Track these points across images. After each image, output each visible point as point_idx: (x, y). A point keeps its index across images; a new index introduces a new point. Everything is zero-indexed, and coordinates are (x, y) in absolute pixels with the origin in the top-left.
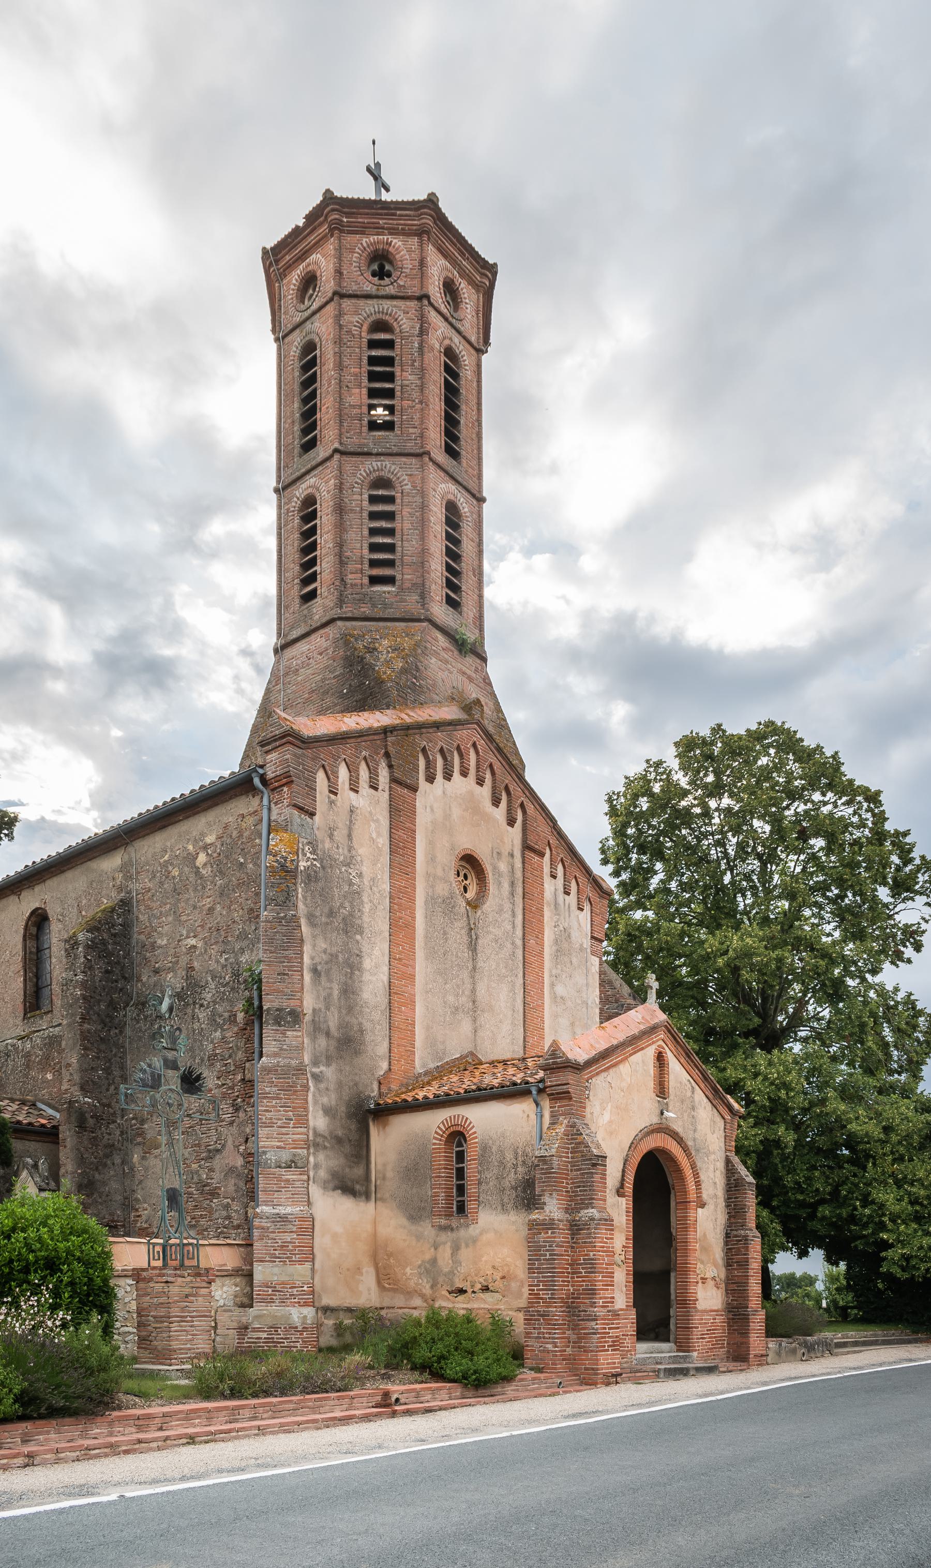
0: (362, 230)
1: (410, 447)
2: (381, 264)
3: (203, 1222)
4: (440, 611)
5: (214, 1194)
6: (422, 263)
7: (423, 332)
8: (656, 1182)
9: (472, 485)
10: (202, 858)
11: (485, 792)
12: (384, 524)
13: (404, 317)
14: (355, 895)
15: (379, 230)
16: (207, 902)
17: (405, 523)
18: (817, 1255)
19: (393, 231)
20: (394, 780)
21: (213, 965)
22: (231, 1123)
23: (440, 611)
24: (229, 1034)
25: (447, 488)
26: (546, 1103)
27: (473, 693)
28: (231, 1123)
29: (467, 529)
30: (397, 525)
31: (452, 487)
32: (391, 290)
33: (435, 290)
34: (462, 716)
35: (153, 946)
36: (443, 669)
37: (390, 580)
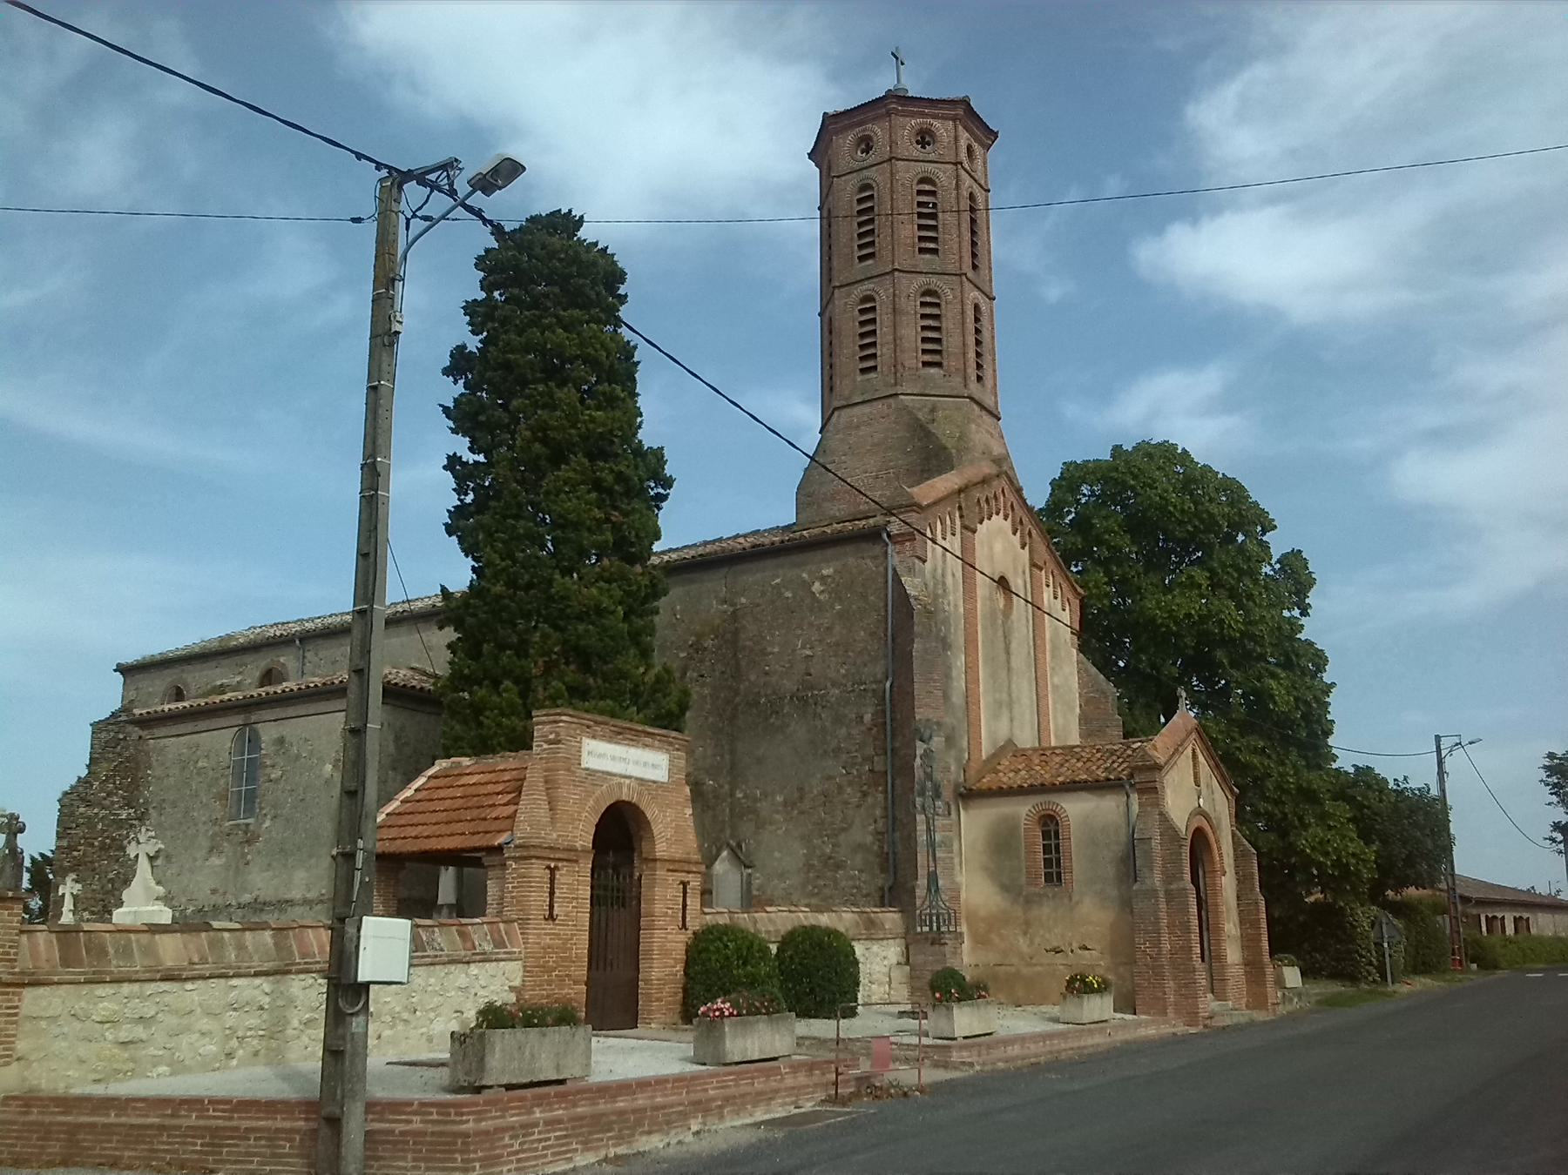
0: (913, 115)
1: (950, 268)
2: (925, 138)
3: (827, 891)
4: (974, 387)
5: (839, 866)
6: (956, 139)
7: (958, 187)
8: (1200, 843)
9: (986, 289)
10: (817, 587)
11: (1008, 524)
12: (931, 323)
13: (944, 175)
14: (946, 622)
15: (923, 115)
16: (826, 622)
17: (949, 324)
18: (459, 573)
19: (935, 117)
20: (964, 527)
21: (832, 675)
22: (859, 806)
23: (974, 387)
24: (854, 732)
25: (974, 294)
26: (1134, 797)
27: (997, 450)
28: (859, 806)
29: (985, 320)
30: (941, 236)
31: (977, 293)
32: (932, 157)
33: (963, 156)
34: (993, 470)
35: (764, 652)
36: (980, 433)
37: (939, 365)
